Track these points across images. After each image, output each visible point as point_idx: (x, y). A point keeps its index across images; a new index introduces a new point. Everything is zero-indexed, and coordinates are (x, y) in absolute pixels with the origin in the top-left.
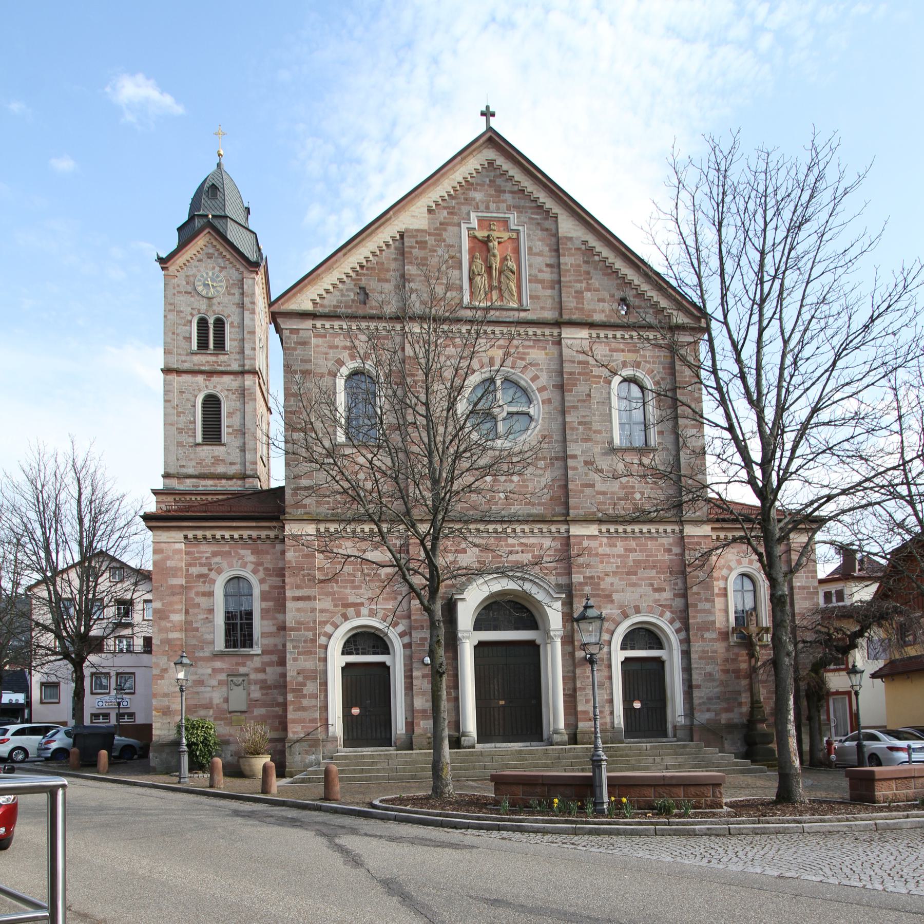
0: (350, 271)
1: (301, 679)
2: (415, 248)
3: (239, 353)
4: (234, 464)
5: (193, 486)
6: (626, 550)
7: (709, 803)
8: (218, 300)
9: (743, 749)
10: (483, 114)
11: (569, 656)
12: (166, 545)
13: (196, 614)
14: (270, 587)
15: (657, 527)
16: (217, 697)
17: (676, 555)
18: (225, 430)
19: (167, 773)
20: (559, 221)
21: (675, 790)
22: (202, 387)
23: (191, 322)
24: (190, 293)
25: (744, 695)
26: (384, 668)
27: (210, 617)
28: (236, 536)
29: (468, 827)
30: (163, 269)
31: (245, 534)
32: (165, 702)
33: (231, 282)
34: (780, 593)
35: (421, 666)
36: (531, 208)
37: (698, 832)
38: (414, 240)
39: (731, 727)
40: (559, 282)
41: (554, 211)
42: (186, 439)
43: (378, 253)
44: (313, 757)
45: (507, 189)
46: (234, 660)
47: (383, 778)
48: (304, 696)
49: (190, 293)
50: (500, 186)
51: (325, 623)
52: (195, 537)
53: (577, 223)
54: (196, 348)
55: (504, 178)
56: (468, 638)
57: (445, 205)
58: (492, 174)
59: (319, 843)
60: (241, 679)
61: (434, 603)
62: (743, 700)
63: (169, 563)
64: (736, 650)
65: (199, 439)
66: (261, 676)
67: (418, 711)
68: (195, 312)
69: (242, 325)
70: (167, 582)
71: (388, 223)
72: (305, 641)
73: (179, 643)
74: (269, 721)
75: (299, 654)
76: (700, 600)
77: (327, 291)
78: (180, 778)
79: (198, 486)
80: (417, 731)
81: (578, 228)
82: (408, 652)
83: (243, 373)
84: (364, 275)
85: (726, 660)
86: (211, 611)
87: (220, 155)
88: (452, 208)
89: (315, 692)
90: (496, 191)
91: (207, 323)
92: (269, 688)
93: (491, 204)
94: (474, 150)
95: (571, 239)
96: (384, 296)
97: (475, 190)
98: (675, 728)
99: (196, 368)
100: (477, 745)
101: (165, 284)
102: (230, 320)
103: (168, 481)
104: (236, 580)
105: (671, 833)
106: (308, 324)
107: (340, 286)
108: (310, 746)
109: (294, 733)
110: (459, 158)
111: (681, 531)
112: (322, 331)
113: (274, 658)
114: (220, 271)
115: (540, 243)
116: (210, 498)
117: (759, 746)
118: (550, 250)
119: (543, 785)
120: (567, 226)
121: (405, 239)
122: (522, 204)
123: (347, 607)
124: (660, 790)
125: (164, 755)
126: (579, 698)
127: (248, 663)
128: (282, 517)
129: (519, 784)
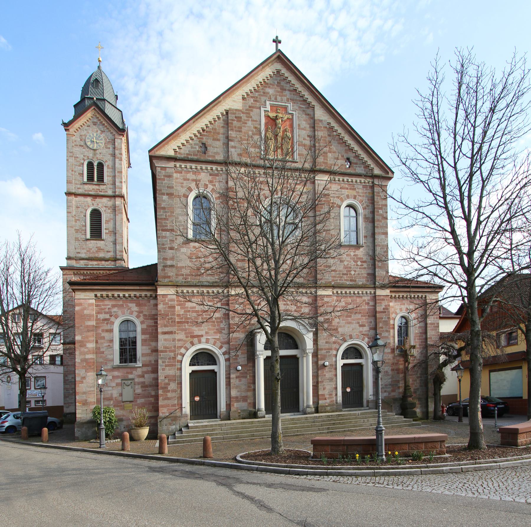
0: (196, 133)
1: (167, 381)
2: (235, 120)
3: (112, 184)
4: (109, 252)
5: (85, 265)
6: (346, 303)
7: (438, 452)
8: (100, 151)
9: (400, 412)
10: (274, 41)
11: (315, 363)
12: (84, 301)
13: (102, 343)
14: (147, 326)
15: (362, 290)
16: (115, 393)
17: (371, 306)
18: (104, 231)
19: (85, 440)
20: (315, 110)
21: (420, 445)
22: (90, 205)
23: (83, 164)
24: (83, 146)
25: (401, 382)
26: (213, 373)
27: (111, 344)
28: (127, 295)
29: (307, 474)
30: (66, 130)
31: (133, 294)
32: (84, 397)
33: (108, 140)
34: (477, 329)
35: (236, 371)
36: (300, 101)
37: (445, 472)
38: (234, 116)
39: (395, 400)
40: (314, 146)
41: (313, 104)
42: (81, 236)
43: (213, 122)
44: (174, 427)
45: (287, 88)
46: (125, 370)
47: (220, 438)
48: (169, 391)
49: (83, 146)
50: (283, 86)
51: (181, 347)
52: (102, 296)
53: (325, 112)
54: (86, 180)
55: (285, 81)
56: (262, 354)
57: (252, 95)
58: (279, 78)
59: (223, 491)
60: (130, 382)
61: (274, 337)
62: (401, 385)
63: (86, 312)
64: (398, 358)
65: (88, 236)
66: (142, 380)
67: (233, 398)
68: (86, 158)
69: (114, 168)
70: (84, 324)
71: (219, 104)
72: (169, 359)
73: (92, 361)
74: (147, 406)
75: (166, 366)
76: (383, 331)
77: (183, 145)
78: (101, 445)
79: (88, 265)
80: (233, 409)
81: (325, 115)
82: (228, 363)
83: (115, 197)
84: (205, 135)
85: (393, 364)
86: (112, 341)
87: (99, 61)
88: (255, 97)
89: (175, 388)
90: (281, 89)
91: (93, 165)
92: (147, 386)
93: (278, 97)
94: (269, 63)
95: (321, 121)
96: (216, 150)
97: (269, 87)
98: (368, 402)
99: (86, 193)
100: (266, 416)
101: (67, 140)
102: (107, 164)
103: (69, 262)
104: (126, 322)
105: (430, 473)
106: (172, 164)
107: (191, 141)
108: (172, 421)
109: (163, 413)
110: (261, 67)
111: (375, 293)
112: (180, 169)
113: (149, 369)
114: (101, 134)
115: (305, 122)
116: (101, 272)
117: (409, 410)
118: (310, 127)
119: (344, 445)
120: (320, 113)
121: (229, 115)
122: (295, 98)
123: (194, 338)
124: (412, 445)
125: (84, 429)
126: (320, 387)
127: (134, 372)
128: (156, 284)
129: (328, 445)
